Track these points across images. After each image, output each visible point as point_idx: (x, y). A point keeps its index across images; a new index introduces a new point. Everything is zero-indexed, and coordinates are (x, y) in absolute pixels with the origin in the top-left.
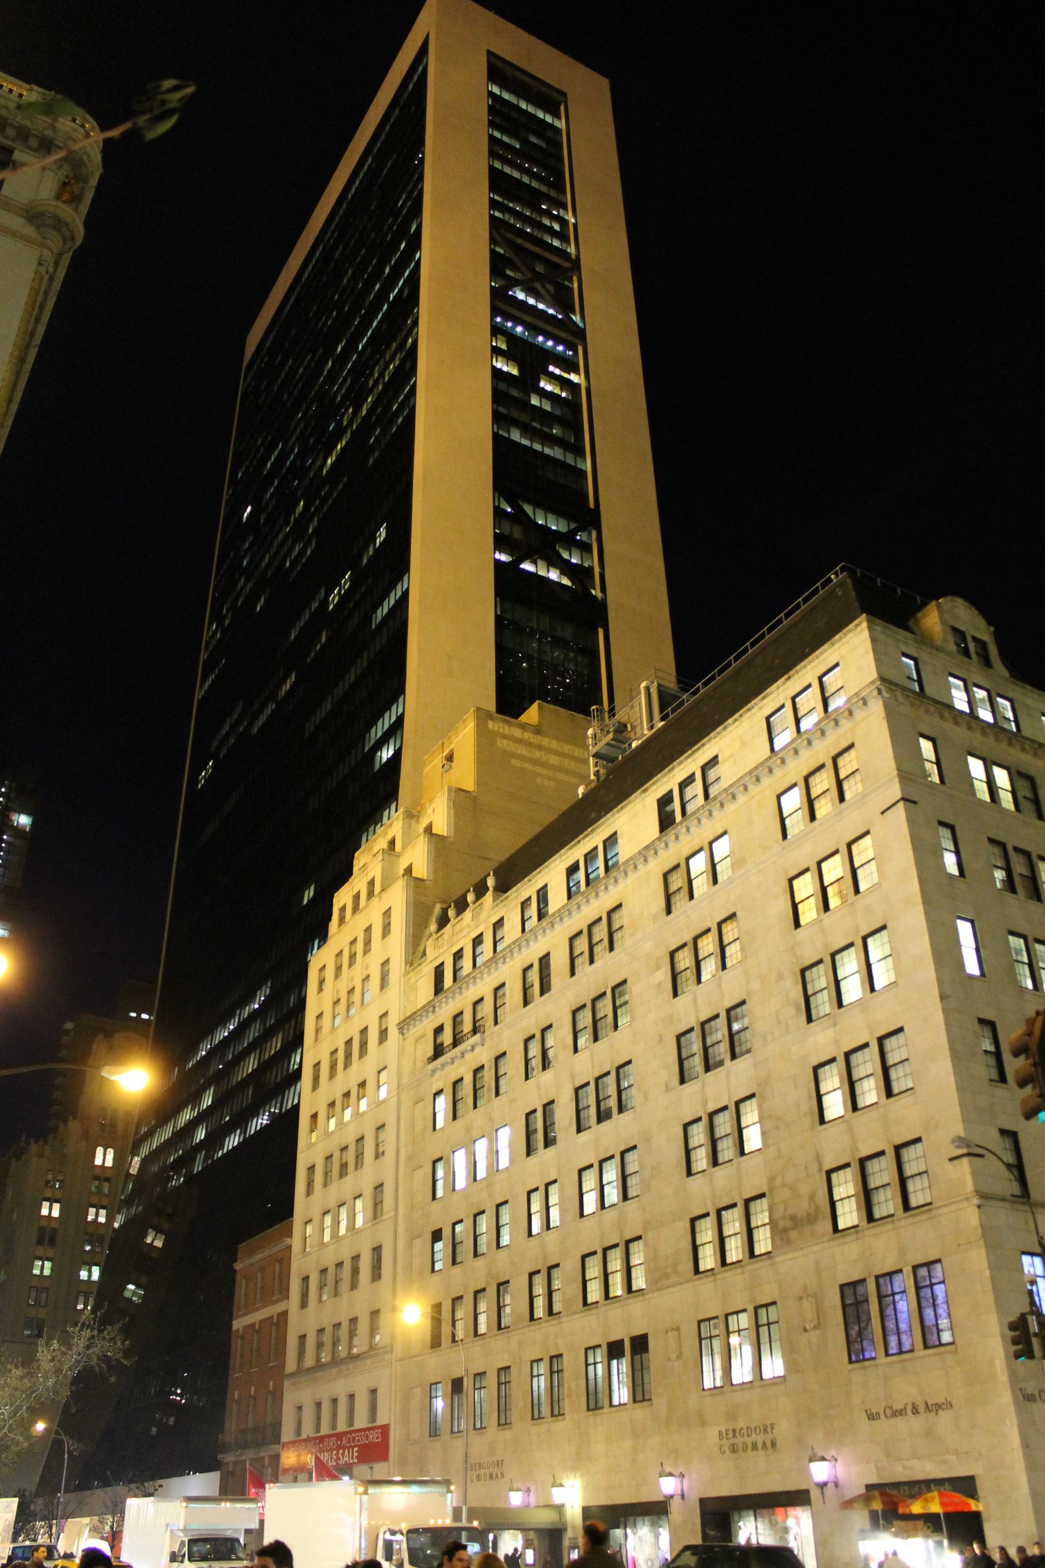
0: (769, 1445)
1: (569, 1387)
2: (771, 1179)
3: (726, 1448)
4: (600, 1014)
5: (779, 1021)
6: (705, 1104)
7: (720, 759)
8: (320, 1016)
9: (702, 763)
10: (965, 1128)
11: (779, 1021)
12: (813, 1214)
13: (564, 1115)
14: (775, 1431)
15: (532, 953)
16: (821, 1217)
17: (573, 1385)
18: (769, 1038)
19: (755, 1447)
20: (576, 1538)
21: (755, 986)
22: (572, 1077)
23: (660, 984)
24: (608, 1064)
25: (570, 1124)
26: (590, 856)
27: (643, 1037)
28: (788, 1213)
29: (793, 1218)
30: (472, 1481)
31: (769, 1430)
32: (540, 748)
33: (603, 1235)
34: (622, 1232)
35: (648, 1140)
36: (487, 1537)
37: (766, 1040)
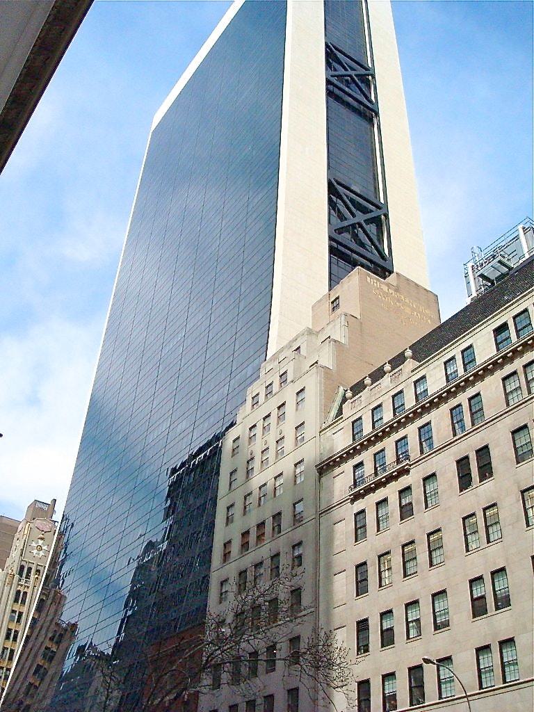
32: (399, 301)
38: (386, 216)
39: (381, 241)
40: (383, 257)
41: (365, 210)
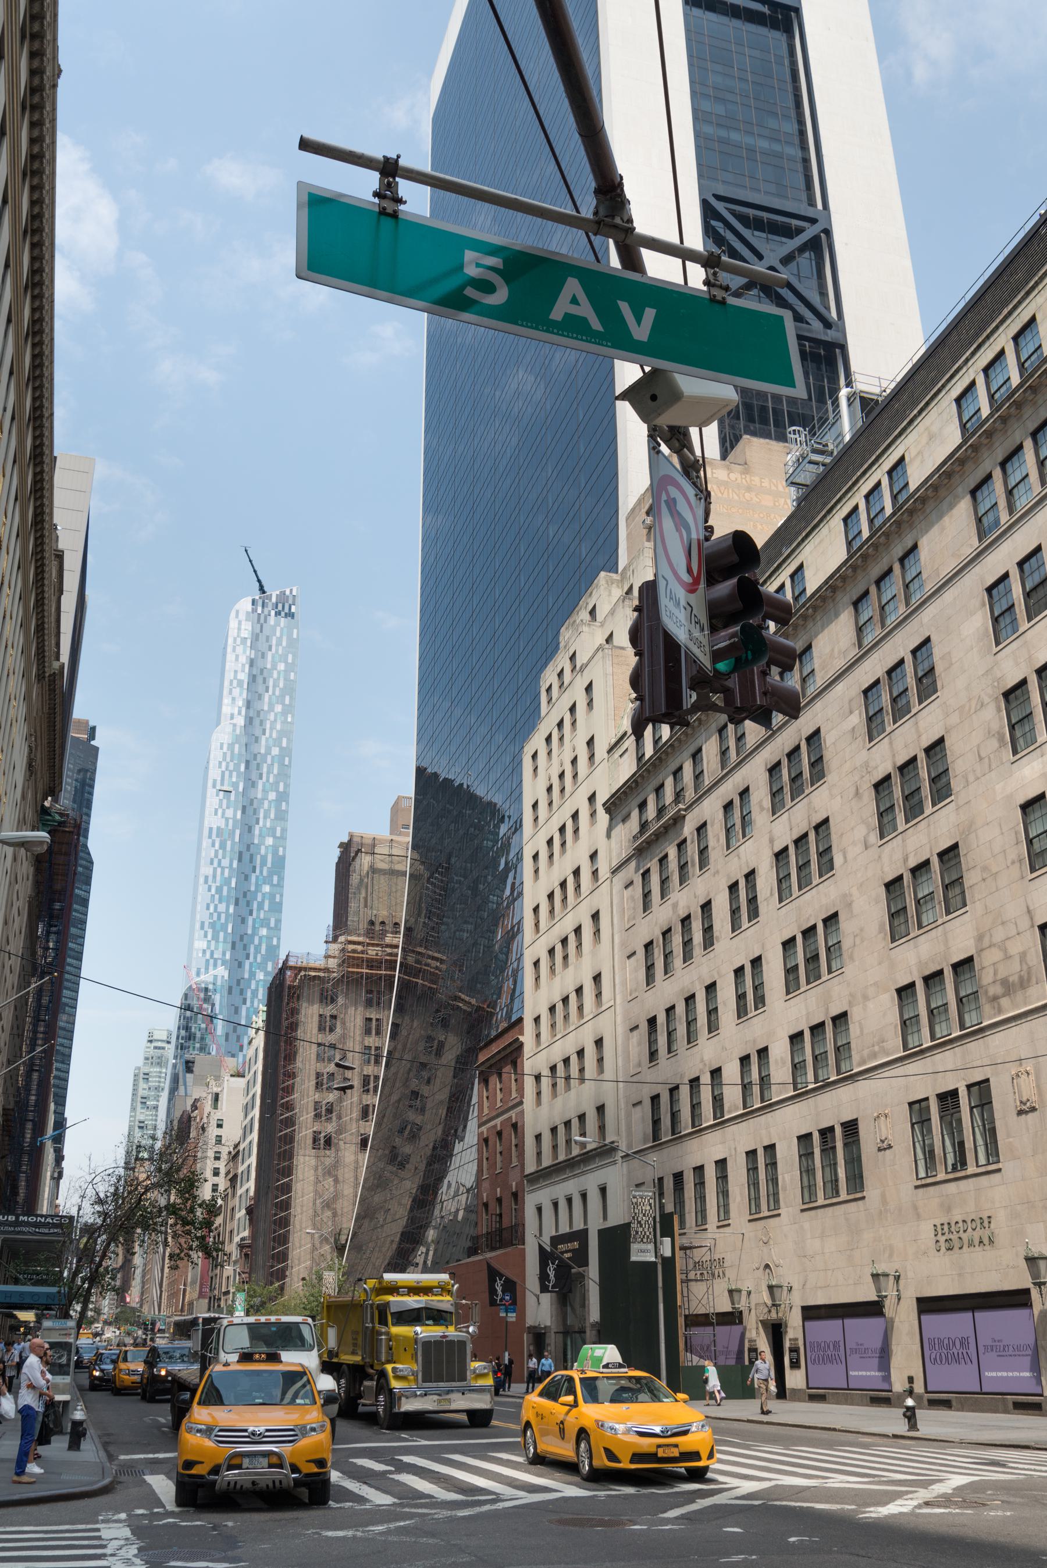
0: (986, 1241)
1: (783, 1178)
2: (980, 938)
3: (942, 1243)
4: (813, 953)
5: (981, 759)
6: (906, 860)
7: (907, 459)
8: (535, 806)
9: (1012, 335)
10: (963, 498)
11: (981, 759)
12: (1026, 978)
13: (766, 883)
14: (992, 1225)
15: (729, 789)
16: (1034, 980)
17: (787, 1177)
18: (971, 778)
19: (971, 1244)
20: (796, 1339)
21: (954, 719)
22: (771, 841)
23: (854, 728)
24: (816, 918)
25: (772, 894)
26: (793, 753)
27: (868, 980)
28: (999, 977)
29: (1004, 982)
30: (696, 912)
31: (986, 1224)
32: (749, 489)
33: (808, 1014)
34: (827, 1009)
35: (850, 905)
36: (725, 262)
37: (967, 781)
38: (828, 232)
39: (823, 294)
40: (827, 324)
41: (789, 233)
